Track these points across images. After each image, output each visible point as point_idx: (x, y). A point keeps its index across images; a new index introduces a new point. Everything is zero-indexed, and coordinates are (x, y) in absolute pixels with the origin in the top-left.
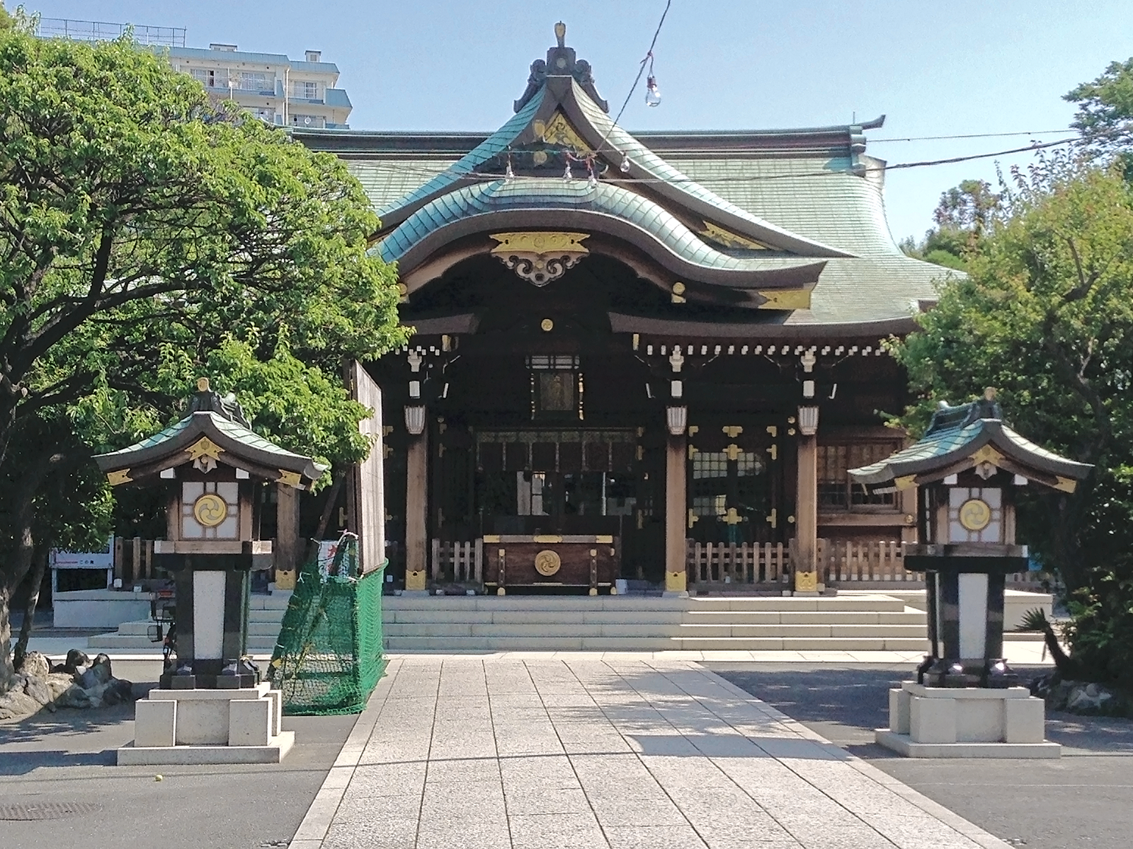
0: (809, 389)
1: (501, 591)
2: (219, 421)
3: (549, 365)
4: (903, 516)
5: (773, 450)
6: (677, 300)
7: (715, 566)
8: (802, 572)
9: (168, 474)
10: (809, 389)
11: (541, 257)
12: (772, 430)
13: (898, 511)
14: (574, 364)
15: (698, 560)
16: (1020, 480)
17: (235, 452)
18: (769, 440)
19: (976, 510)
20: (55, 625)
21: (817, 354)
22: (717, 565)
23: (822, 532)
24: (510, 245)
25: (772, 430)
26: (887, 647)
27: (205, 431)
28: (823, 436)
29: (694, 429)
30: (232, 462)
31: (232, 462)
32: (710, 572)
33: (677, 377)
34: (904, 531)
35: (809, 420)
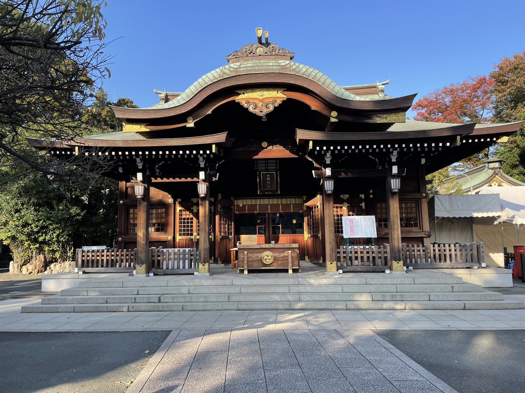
0: (395, 170)
3: (265, 167)
4: (424, 233)
5: (363, 204)
6: (333, 120)
7: (374, 258)
8: (139, 264)
10: (395, 170)
11: (262, 101)
12: (362, 196)
13: (421, 230)
14: (276, 167)
15: (342, 255)
18: (361, 201)
19: (268, 261)
20: (42, 291)
22: (357, 257)
23: (404, 239)
24: (243, 98)
25: (362, 196)
26: (467, 307)
28: (402, 191)
32: (90, 264)
33: (394, 164)
34: (425, 239)
35: (395, 184)
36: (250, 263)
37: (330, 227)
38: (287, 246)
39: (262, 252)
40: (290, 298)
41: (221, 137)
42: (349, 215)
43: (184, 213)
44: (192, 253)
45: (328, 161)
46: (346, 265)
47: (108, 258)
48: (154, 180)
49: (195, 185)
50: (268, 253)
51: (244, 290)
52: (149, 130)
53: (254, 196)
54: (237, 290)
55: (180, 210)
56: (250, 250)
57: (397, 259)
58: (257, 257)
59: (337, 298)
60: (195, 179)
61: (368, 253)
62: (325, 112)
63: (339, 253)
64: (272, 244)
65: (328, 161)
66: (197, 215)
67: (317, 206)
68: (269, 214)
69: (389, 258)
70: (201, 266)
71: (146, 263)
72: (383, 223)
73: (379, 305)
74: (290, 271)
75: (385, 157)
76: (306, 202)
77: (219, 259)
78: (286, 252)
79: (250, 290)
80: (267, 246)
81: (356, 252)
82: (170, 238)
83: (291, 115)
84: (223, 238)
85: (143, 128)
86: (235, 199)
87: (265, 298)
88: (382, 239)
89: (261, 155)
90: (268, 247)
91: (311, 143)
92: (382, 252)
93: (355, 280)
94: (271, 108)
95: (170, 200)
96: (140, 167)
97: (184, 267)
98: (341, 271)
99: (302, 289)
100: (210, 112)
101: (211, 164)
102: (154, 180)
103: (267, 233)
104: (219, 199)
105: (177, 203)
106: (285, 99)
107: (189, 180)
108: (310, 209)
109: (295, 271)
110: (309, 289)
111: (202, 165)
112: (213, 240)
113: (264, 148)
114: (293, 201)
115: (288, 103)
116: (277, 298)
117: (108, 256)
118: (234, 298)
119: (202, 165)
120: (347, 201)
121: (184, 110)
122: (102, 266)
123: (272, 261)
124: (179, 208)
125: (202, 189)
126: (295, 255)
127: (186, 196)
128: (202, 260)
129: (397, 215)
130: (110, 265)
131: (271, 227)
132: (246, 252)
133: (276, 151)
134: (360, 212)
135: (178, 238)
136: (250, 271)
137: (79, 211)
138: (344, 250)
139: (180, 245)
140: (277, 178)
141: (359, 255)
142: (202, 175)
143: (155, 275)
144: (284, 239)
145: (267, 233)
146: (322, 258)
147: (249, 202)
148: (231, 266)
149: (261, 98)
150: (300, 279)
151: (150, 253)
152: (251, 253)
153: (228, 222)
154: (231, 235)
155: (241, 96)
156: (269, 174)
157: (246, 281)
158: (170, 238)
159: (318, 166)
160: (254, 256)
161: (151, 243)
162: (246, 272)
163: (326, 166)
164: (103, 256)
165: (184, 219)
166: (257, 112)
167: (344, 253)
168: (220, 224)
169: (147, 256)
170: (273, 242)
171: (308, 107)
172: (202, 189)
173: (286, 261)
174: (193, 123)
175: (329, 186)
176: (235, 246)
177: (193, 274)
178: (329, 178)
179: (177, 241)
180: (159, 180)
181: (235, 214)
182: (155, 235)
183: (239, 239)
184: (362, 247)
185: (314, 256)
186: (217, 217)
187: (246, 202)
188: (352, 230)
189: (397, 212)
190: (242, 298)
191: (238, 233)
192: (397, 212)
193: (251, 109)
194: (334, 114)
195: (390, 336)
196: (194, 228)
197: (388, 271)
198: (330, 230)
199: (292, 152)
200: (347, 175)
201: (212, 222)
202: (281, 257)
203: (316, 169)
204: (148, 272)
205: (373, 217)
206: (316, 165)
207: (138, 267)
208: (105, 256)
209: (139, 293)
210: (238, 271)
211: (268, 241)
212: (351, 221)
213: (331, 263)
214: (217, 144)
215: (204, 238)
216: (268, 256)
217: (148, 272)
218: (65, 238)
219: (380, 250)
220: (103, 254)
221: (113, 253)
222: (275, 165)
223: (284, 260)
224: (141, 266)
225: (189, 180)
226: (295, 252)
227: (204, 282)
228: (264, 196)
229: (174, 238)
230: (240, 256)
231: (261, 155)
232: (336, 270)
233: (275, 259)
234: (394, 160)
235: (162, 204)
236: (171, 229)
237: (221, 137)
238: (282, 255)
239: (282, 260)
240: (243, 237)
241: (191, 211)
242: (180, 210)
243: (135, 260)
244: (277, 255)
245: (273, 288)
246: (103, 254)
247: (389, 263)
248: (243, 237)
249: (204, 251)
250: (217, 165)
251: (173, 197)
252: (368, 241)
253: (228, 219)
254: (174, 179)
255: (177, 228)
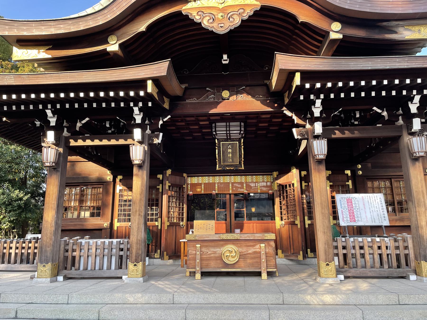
3: (227, 131)
5: (350, 183)
6: (333, 36)
12: (348, 172)
14: (241, 130)
19: (230, 259)
36: (204, 262)
37: (322, 208)
38: (258, 236)
39: (223, 246)
43: (125, 193)
44: (122, 246)
47: (17, 251)
50: (230, 247)
52: (50, 56)
53: (213, 172)
55: (120, 190)
58: (215, 253)
61: (379, 248)
63: (336, 247)
64: (237, 234)
67: (293, 184)
68: (230, 194)
69: (412, 256)
70: (131, 266)
71: (53, 261)
74: (264, 276)
76: (277, 179)
77: (165, 253)
78: (258, 246)
80: (230, 236)
81: (361, 248)
82: (106, 224)
85: (41, 54)
86: (188, 176)
89: (220, 109)
90: (231, 238)
91: (298, 76)
92: (401, 248)
93: (380, 297)
94: (237, 21)
95: (109, 177)
96: (53, 124)
97: (109, 267)
98: (342, 277)
100: (142, 28)
103: (228, 219)
104: (168, 175)
105: (118, 180)
106: (258, 8)
108: (283, 187)
109: (270, 274)
111: (138, 119)
112: (159, 228)
113: (224, 99)
117: (17, 248)
119: (138, 119)
121: (101, 21)
122: (9, 262)
123: (236, 259)
128: (134, 258)
129: (422, 191)
130: (19, 261)
132: (198, 246)
134: (359, 187)
135: (116, 224)
136: (204, 274)
137: (22, 195)
138: (344, 244)
139: (119, 234)
140: (240, 150)
142: (137, 133)
143: (66, 278)
145: (228, 219)
146: (301, 252)
148: (179, 262)
149: (221, 6)
150: (286, 295)
151: (62, 246)
152: (206, 246)
153: (179, 205)
154: (182, 221)
155: (190, 5)
156: (230, 144)
158: (106, 224)
159: (301, 122)
160: (210, 251)
162: (198, 276)
163: (313, 120)
164: (11, 248)
165: (125, 201)
167: (344, 248)
170: (238, 231)
172: (137, 153)
173: (256, 260)
174: (117, 45)
176: (184, 238)
177: (121, 278)
179: (115, 228)
181: (188, 195)
183: (192, 227)
184: (369, 239)
187: (202, 180)
189: (422, 187)
192: (422, 187)
194: (336, 26)
198: (323, 213)
199: (263, 102)
200: (344, 133)
201: (153, 201)
202: (250, 254)
203: (297, 126)
204: (55, 274)
208: (14, 248)
209: (19, 316)
210: (188, 274)
211: (230, 230)
213: (328, 265)
214: (156, 81)
215: (139, 224)
216: (231, 252)
217: (55, 274)
218: (7, 225)
219: (397, 244)
220: (11, 245)
221: (24, 245)
222: (239, 128)
223: (254, 258)
224: (44, 266)
226: (269, 245)
228: (224, 172)
229: (112, 224)
232: (334, 275)
233: (242, 256)
235: (100, 182)
237: (161, 68)
238: (251, 250)
239: (252, 258)
242: (120, 190)
244: (244, 250)
245: (241, 312)
246: (11, 245)
247: (413, 264)
249: (137, 243)
250: (161, 122)
251: (112, 173)
252: (374, 230)
253: (179, 200)
254: (101, 140)
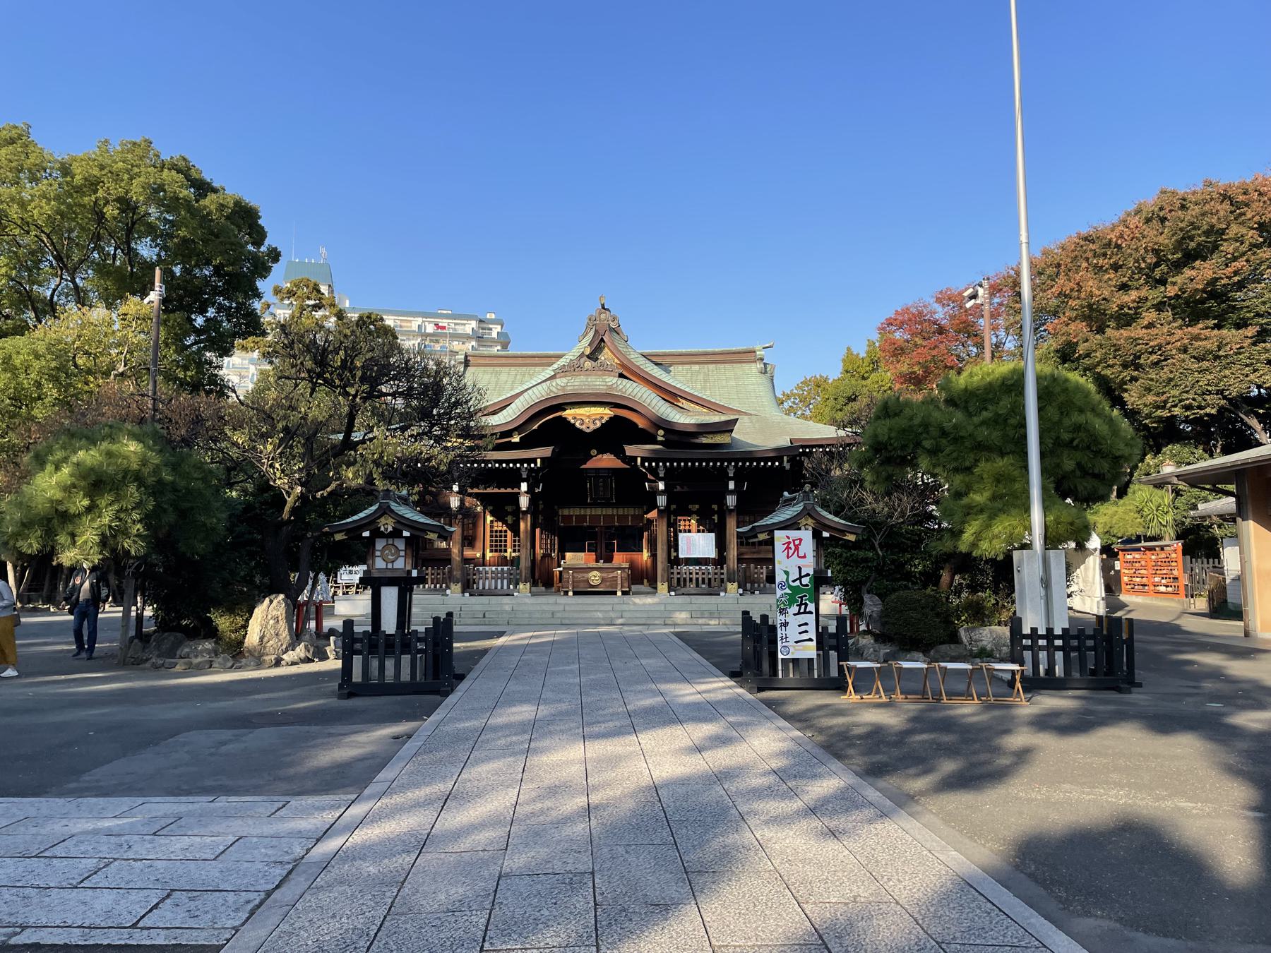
0: (731, 485)
1: (571, 593)
2: (394, 506)
5: (716, 517)
6: (660, 438)
9: (366, 534)
10: (731, 485)
16: (826, 534)
17: (402, 522)
18: (714, 513)
21: (736, 466)
24: (569, 414)
25: (715, 507)
27: (385, 511)
29: (673, 507)
30: (400, 527)
31: (400, 527)
33: (731, 479)
35: (731, 501)
40: (612, 615)
41: (547, 451)
42: (699, 531)
45: (662, 475)
46: (677, 585)
48: (470, 491)
49: (516, 497)
51: (567, 608)
53: (583, 504)
54: (561, 608)
56: (576, 569)
57: (731, 580)
59: (657, 615)
60: (516, 490)
62: (652, 431)
65: (662, 475)
66: (516, 532)
72: (721, 545)
73: (695, 621)
74: (619, 593)
75: (723, 477)
79: (573, 608)
83: (619, 431)
84: (544, 556)
87: (587, 615)
88: (720, 561)
89: (589, 465)
94: (598, 424)
99: (625, 607)
101: (533, 480)
102: (470, 491)
107: (509, 490)
109: (624, 593)
110: (632, 607)
114: (631, 511)
115: (615, 420)
116: (600, 615)
118: (559, 615)
120: (697, 513)
124: (489, 518)
125: (524, 502)
126: (625, 575)
127: (504, 508)
131: (604, 541)
133: (607, 461)
135: (489, 555)
136: (575, 593)
141: (694, 576)
142: (524, 487)
144: (619, 558)
147: (576, 512)
155: (568, 412)
157: (569, 602)
161: (467, 561)
162: (571, 593)
166: (584, 427)
168: (541, 539)
169: (463, 574)
171: (635, 425)
172: (524, 502)
175: (662, 501)
178: (662, 493)
180: (475, 490)
182: (468, 553)
183: (564, 558)
185: (641, 578)
186: (538, 531)
188: (689, 549)
190: (566, 615)
191: (562, 552)
193: (578, 425)
195: (677, 634)
196: (509, 543)
197: (722, 594)
205: (713, 535)
206: (650, 477)
207: (453, 586)
212: (688, 538)
225: (509, 490)
227: (527, 601)
228: (595, 505)
229: (484, 555)
230: (565, 576)
231: (589, 465)
234: (731, 475)
236: (479, 544)
237: (547, 451)
240: (568, 555)
241: (505, 522)
243: (449, 579)
248: (568, 555)
255: (488, 543)
